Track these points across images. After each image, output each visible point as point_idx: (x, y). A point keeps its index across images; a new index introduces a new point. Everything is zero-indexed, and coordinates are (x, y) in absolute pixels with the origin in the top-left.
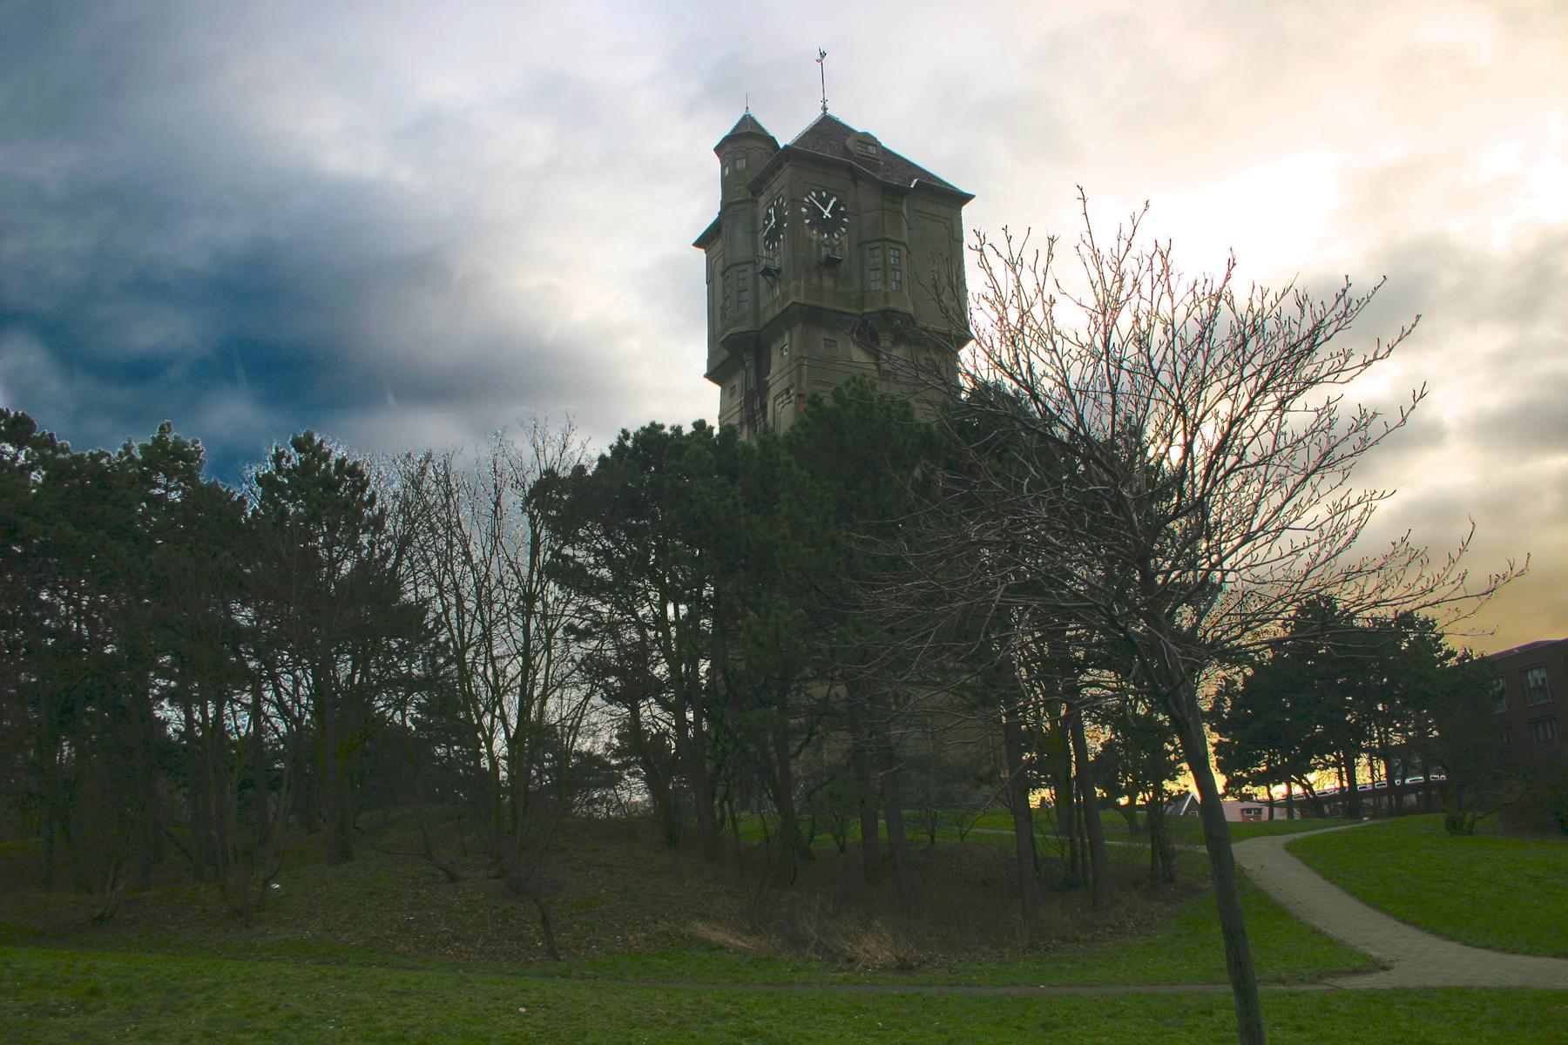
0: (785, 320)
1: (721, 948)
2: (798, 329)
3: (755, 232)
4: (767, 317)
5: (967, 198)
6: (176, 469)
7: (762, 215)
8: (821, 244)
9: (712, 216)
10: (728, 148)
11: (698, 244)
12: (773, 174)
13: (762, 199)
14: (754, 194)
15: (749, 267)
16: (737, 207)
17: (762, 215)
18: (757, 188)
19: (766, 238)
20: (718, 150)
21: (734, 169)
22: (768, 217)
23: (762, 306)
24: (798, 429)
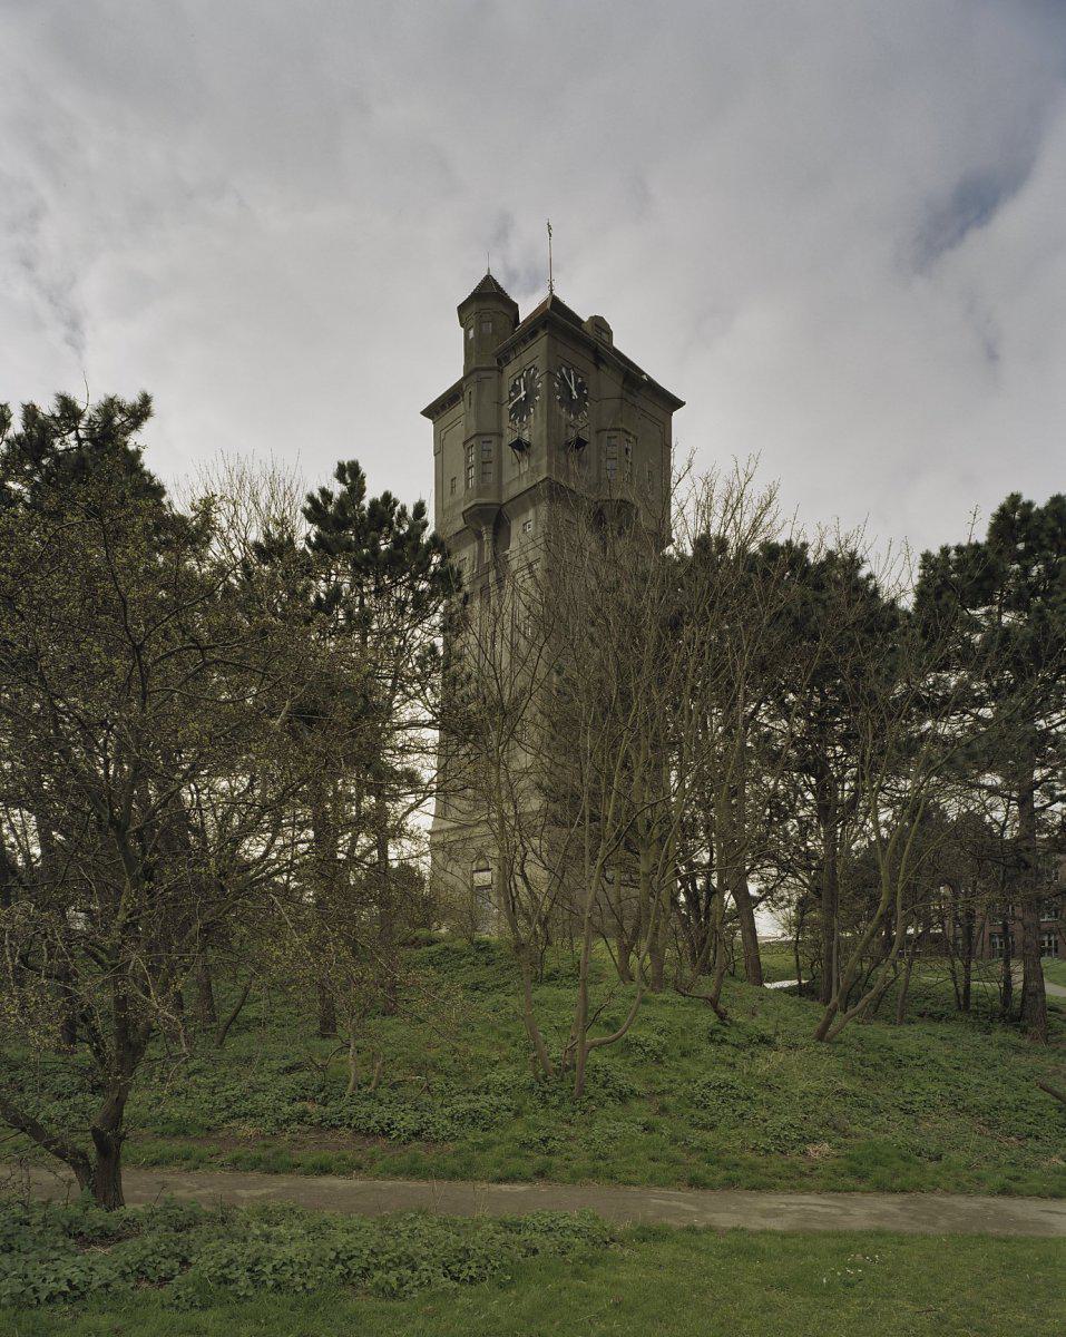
0: (528, 498)
1: (396, 1174)
2: (543, 509)
3: (500, 404)
4: (513, 490)
5: (678, 404)
6: (900, 803)
7: (508, 385)
8: (569, 425)
9: (457, 374)
10: (474, 308)
11: (428, 413)
12: (525, 342)
13: (509, 370)
14: (499, 362)
15: (494, 439)
16: (483, 374)
17: (508, 385)
18: (503, 359)
19: (511, 411)
20: (462, 308)
21: (479, 334)
22: (516, 389)
23: (505, 480)
24: (953, 555)
